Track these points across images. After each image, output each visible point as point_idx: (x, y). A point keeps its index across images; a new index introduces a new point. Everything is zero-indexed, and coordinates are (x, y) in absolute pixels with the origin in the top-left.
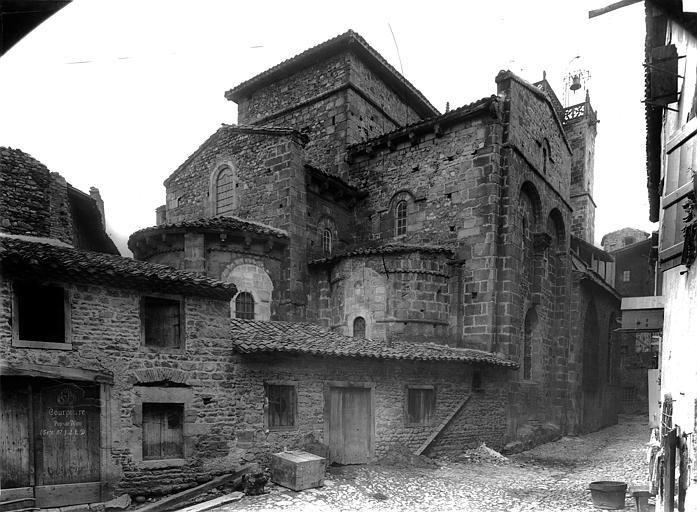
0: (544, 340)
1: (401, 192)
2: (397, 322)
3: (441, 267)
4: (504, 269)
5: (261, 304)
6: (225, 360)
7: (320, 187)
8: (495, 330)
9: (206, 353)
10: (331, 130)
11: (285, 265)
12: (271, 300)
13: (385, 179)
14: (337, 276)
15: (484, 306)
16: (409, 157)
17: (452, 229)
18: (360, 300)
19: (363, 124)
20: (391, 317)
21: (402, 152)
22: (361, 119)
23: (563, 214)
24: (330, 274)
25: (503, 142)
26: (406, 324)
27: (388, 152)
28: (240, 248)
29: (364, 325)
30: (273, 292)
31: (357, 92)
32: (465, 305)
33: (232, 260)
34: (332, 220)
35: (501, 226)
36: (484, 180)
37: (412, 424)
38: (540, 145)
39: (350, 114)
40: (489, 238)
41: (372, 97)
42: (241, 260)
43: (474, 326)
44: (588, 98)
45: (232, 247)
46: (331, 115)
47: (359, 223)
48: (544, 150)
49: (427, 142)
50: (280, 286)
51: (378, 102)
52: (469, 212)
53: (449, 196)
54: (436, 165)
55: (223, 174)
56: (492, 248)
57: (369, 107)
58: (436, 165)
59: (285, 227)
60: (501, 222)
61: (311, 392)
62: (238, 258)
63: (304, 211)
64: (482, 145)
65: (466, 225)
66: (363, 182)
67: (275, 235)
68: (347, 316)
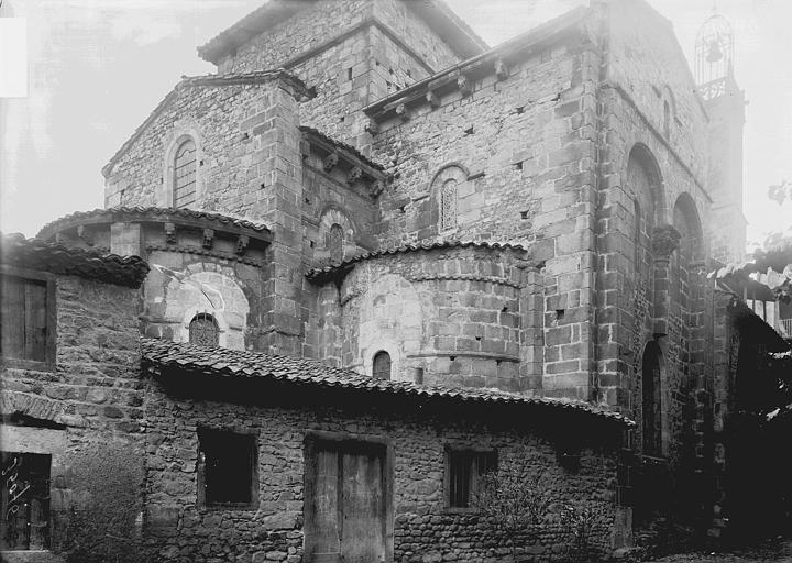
0: (674, 393)
1: (448, 167)
2: (438, 355)
3: (507, 271)
4: (606, 272)
5: (228, 332)
6: (128, 385)
7: (324, 162)
8: (594, 367)
9: (93, 373)
10: (348, 87)
11: (266, 271)
12: (245, 327)
13: (424, 150)
14: (349, 291)
15: (576, 329)
16: (452, 117)
17: (524, 214)
18: (384, 327)
19: (393, 79)
20: (430, 349)
21: (450, 108)
22: (391, 72)
23: (698, 204)
24: (339, 286)
25: (600, 80)
26: (452, 358)
27: (429, 109)
28: (196, 245)
29: (389, 363)
30: (249, 316)
31: (383, 30)
32: (546, 330)
33: (185, 264)
34: (344, 212)
35: (600, 207)
36: (573, 135)
37: (454, 510)
38: (659, 95)
39: (373, 63)
40: (583, 223)
41: (408, 42)
42: (199, 265)
43: (561, 360)
44: (730, 69)
45: (186, 243)
46: (346, 66)
47: (387, 218)
48: (666, 104)
49: (483, 91)
50: (257, 302)
51: (418, 50)
52: (547, 189)
53: (520, 165)
54: (499, 121)
55: (183, 150)
56: (587, 238)
57: (404, 56)
58: (499, 121)
59: (269, 217)
60: (598, 201)
61: (280, 447)
62: (194, 261)
63: (298, 193)
64: (568, 85)
65: (545, 207)
66: (393, 158)
67: (251, 227)
68: (363, 350)
